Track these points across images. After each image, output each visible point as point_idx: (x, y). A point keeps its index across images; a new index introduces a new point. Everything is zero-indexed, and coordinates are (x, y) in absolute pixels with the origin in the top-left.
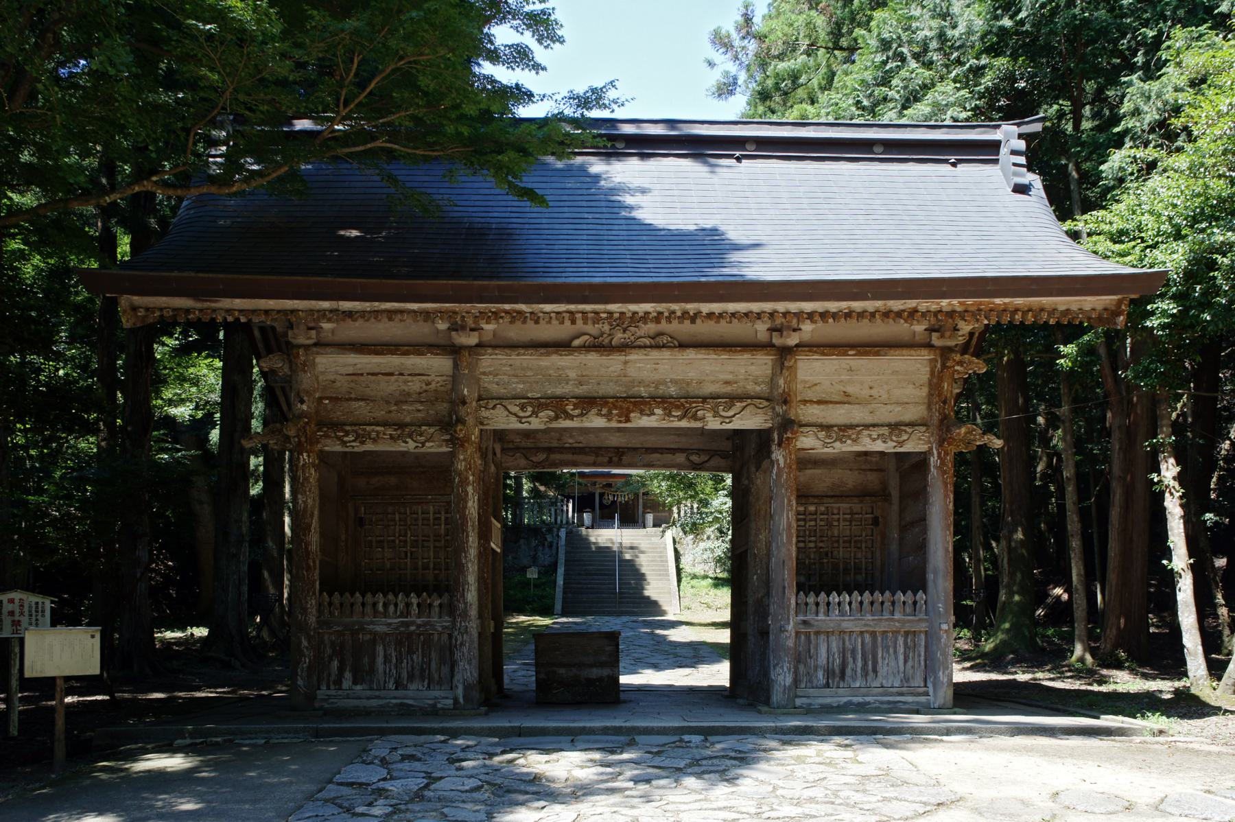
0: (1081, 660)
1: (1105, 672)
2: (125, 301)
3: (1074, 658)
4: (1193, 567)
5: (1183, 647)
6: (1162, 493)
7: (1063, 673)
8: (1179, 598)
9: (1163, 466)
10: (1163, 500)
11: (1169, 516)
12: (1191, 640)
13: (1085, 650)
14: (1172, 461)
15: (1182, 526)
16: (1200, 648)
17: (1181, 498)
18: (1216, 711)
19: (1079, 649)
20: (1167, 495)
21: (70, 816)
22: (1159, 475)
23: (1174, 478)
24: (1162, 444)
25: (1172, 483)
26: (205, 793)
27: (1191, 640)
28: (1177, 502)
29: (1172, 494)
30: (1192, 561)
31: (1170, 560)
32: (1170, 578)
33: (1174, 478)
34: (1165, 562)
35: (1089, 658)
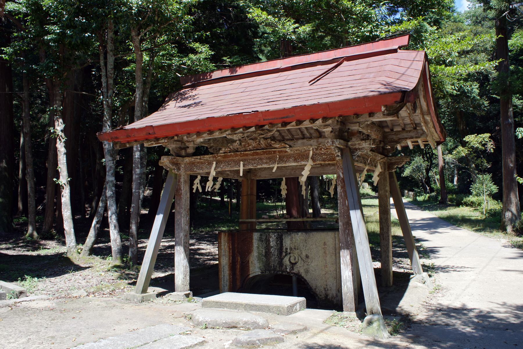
0: (31, 235)
1: (43, 242)
2: (324, 176)
3: (27, 235)
4: (71, 183)
5: (64, 229)
6: (55, 139)
7: (18, 244)
8: (62, 201)
9: (56, 124)
10: (56, 143)
11: (58, 153)
12: (68, 226)
13: (33, 230)
14: (61, 120)
15: (65, 159)
16: (73, 230)
17: (65, 142)
18: (78, 268)
19: (30, 229)
20: (58, 140)
21: (491, 232)
22: (54, 128)
23: (62, 131)
24: (56, 111)
25: (60, 134)
26: (210, 260)
27: (68, 226)
28: (63, 144)
29: (60, 140)
30: (69, 179)
31: (58, 178)
32: (58, 189)
33: (62, 131)
34: (55, 179)
35: (35, 234)
